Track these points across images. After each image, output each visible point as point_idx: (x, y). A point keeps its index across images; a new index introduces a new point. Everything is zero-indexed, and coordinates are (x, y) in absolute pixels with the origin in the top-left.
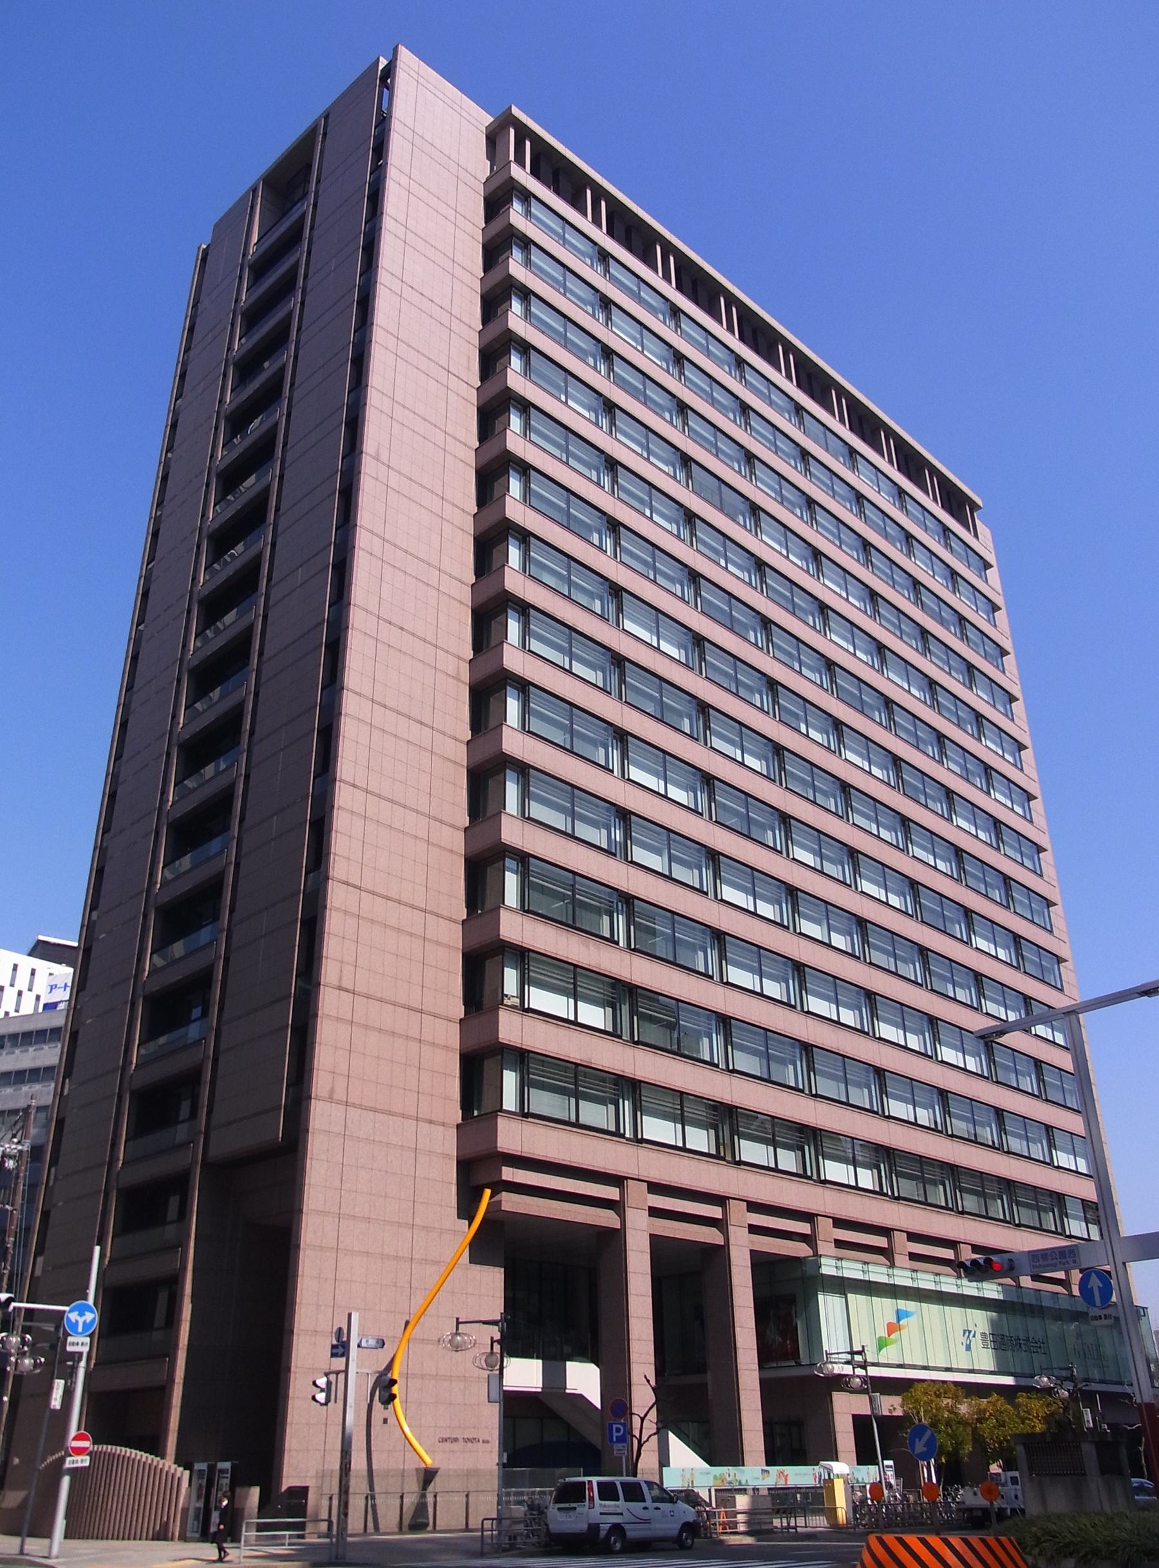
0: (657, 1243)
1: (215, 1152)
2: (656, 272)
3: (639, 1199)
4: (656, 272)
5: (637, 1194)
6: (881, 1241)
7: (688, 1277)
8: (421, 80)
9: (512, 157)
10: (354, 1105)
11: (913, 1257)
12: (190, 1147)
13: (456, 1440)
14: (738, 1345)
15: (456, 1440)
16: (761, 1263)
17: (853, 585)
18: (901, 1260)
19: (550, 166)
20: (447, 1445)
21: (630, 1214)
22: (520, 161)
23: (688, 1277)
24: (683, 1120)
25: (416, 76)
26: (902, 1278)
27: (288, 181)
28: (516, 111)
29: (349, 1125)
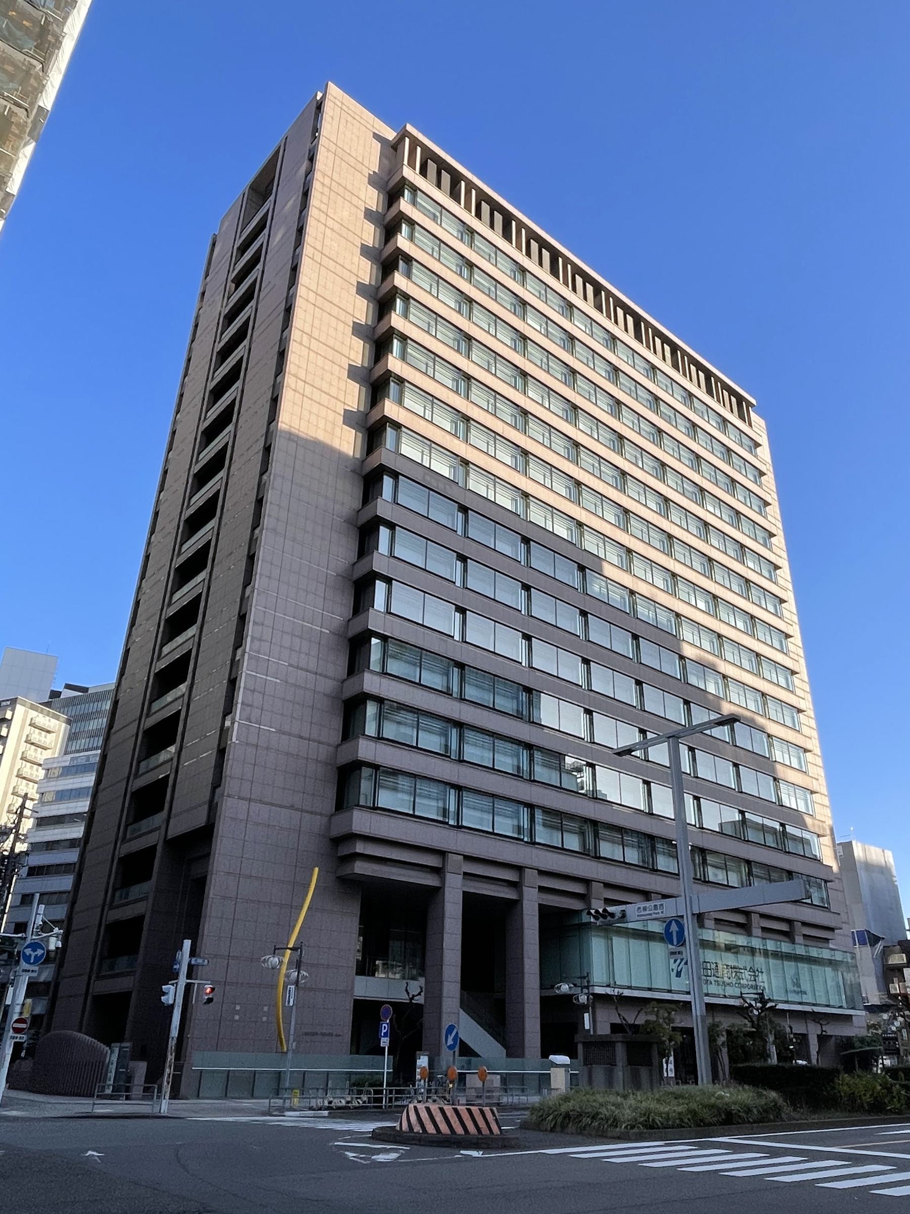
0: (468, 897)
1: (172, 834)
2: (511, 243)
3: (532, 880)
4: (511, 243)
5: (531, 877)
6: (784, 927)
7: (489, 922)
8: (344, 107)
9: (406, 162)
10: (255, 801)
11: (764, 929)
12: (152, 833)
13: (317, 1034)
14: (526, 970)
15: (317, 1034)
16: (545, 912)
17: (724, 507)
18: (799, 939)
19: (430, 163)
20: (308, 1038)
21: (450, 878)
22: (412, 164)
23: (489, 922)
24: (726, 868)
25: (340, 105)
26: (800, 950)
27: (262, 189)
28: (409, 128)
29: (251, 813)
